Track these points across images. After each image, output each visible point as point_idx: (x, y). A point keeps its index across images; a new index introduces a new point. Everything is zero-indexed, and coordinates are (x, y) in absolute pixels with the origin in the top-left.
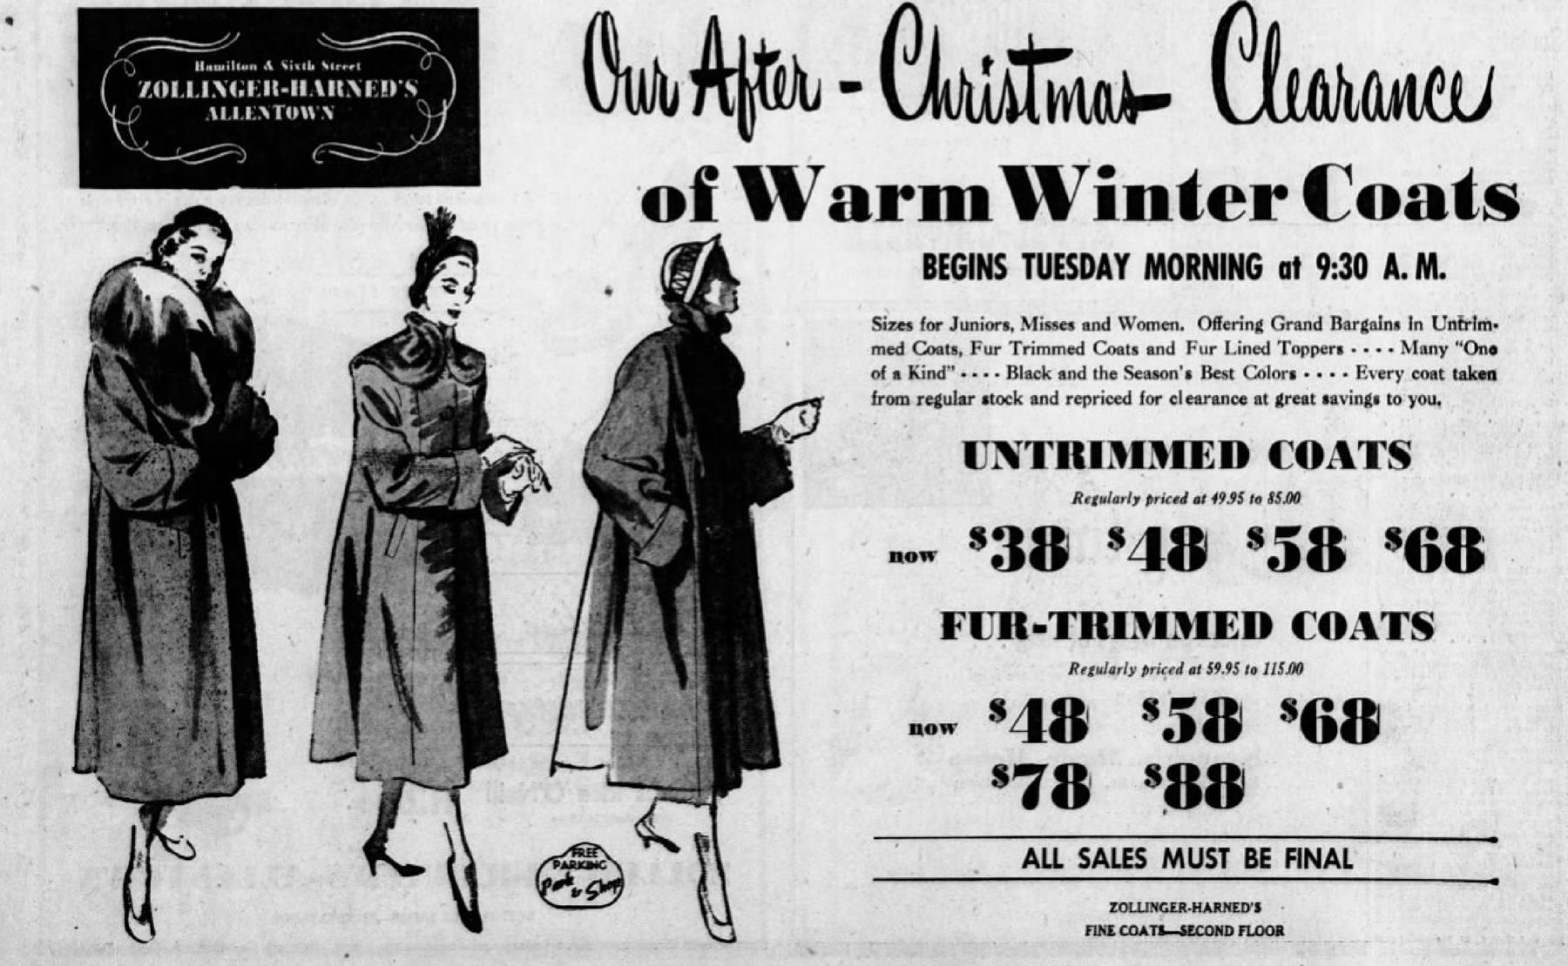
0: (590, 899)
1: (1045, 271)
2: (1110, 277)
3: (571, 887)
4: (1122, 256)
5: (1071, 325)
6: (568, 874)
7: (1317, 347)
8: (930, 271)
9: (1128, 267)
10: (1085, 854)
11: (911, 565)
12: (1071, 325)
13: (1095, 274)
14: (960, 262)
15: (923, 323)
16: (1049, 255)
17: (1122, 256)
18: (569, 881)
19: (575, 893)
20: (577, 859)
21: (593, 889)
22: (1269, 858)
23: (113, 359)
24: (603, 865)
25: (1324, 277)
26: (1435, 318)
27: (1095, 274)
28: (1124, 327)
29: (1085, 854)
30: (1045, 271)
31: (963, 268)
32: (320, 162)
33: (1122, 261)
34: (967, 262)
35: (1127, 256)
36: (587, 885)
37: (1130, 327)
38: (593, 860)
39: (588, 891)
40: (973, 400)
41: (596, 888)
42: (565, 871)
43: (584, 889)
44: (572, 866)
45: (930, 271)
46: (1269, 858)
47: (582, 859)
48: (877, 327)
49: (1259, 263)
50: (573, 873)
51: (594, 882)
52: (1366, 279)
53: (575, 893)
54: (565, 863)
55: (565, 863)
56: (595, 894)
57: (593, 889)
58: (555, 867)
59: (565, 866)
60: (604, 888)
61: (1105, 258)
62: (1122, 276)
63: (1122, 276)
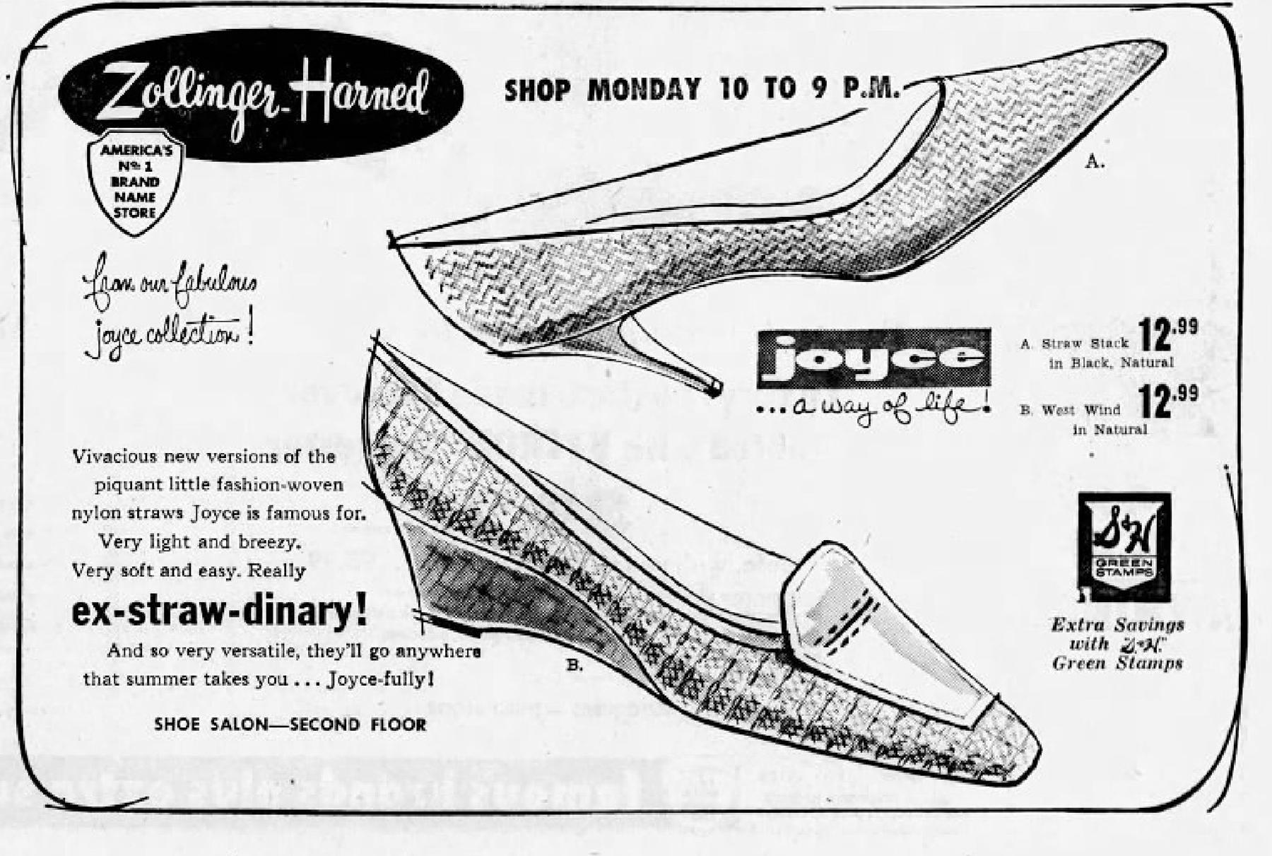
2: (680, 97)
5: (153, 456)
7: (406, 729)
9: (699, 91)
12: (153, 456)
15: (220, 482)
16: (270, 621)
22: (198, 724)
23: (479, 506)
26: (119, 517)
28: (1046, 412)
32: (427, 112)
33: (693, 84)
35: (697, 80)
37: (171, 517)
40: (195, 680)
46: (198, 724)
48: (1121, 666)
61: (675, 81)
62: (693, 96)
63: (693, 96)
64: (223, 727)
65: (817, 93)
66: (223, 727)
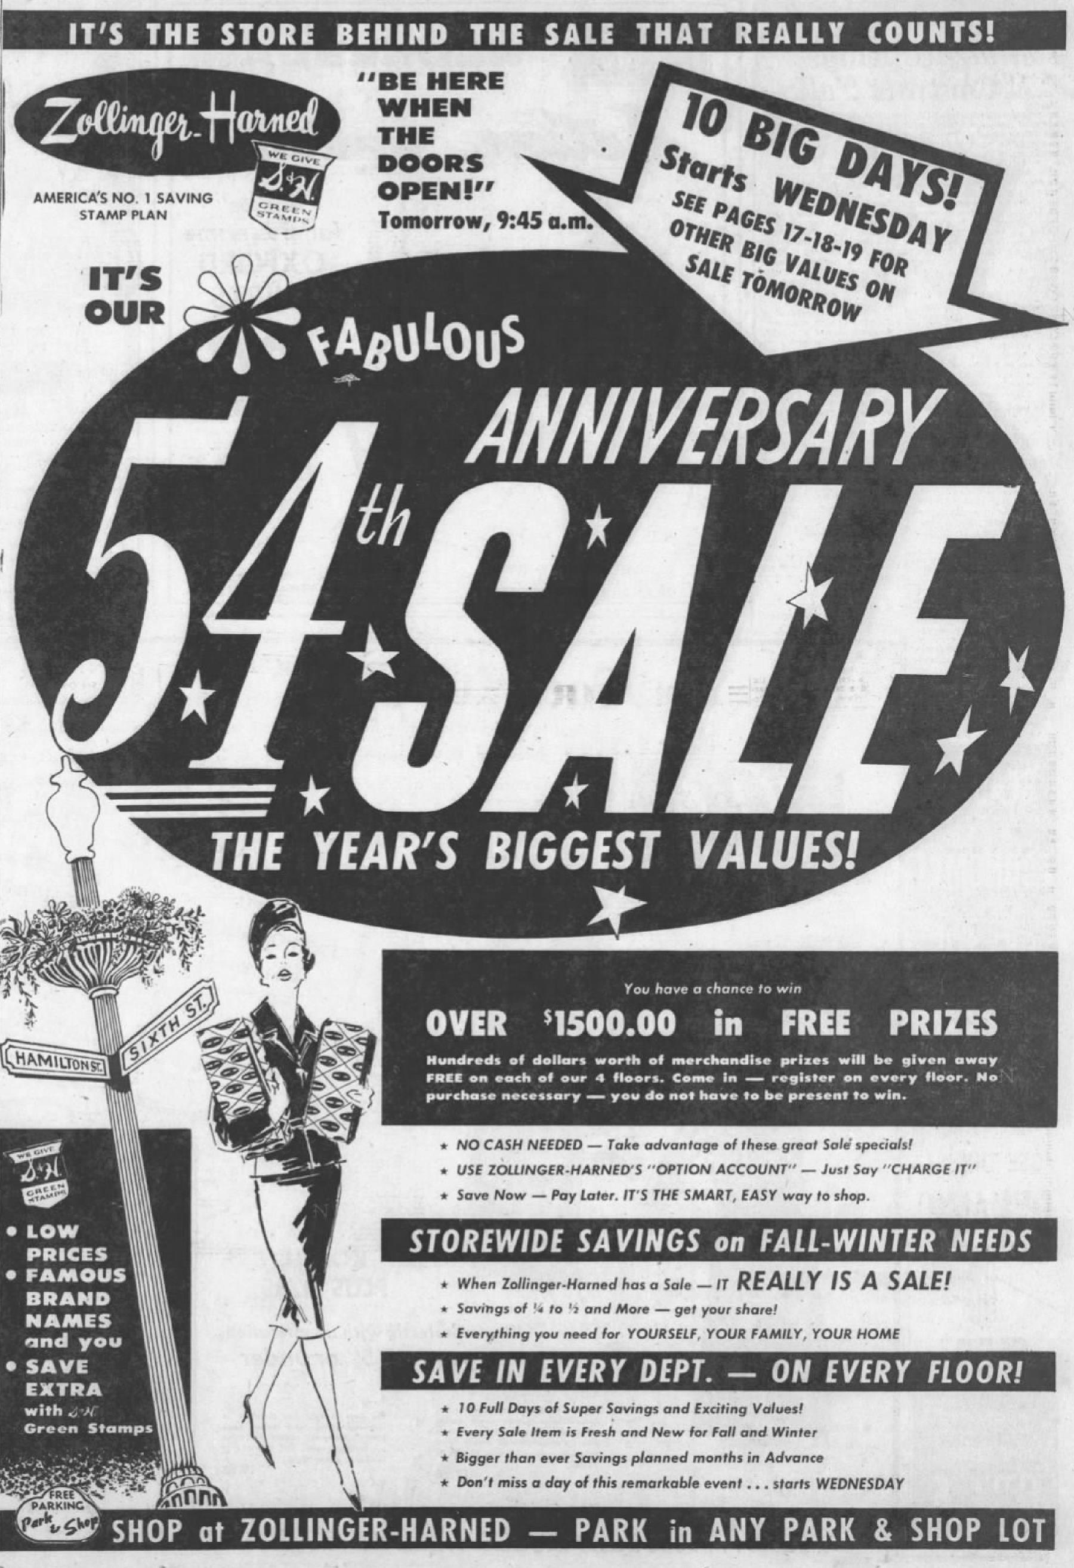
0: (69, 1534)
1: (829, 278)
3: (50, 1524)
4: (814, 1274)
6: (46, 1514)
8: (748, 253)
10: (895, 1276)
11: (468, 1202)
14: (749, 217)
17: (814, 1274)
18: (48, 1519)
19: (53, 1530)
20: (54, 1500)
21: (70, 1525)
24: (80, 1505)
25: (503, 227)
29: (895, 1276)
30: (829, 278)
31: (751, 221)
34: (754, 218)
36: (66, 1521)
38: (71, 1501)
39: (66, 1527)
41: (74, 1524)
42: (43, 1511)
43: (62, 1525)
44: (50, 1506)
45: (748, 253)
47: (59, 1500)
49: (813, 144)
50: (50, 1512)
51: (73, 1520)
52: (718, 138)
53: (53, 1530)
54: (43, 1504)
55: (43, 1504)
56: (74, 1530)
57: (70, 1525)
58: (34, 1508)
59: (43, 1506)
60: (81, 1525)
64: (906, 1285)
65: (500, 224)
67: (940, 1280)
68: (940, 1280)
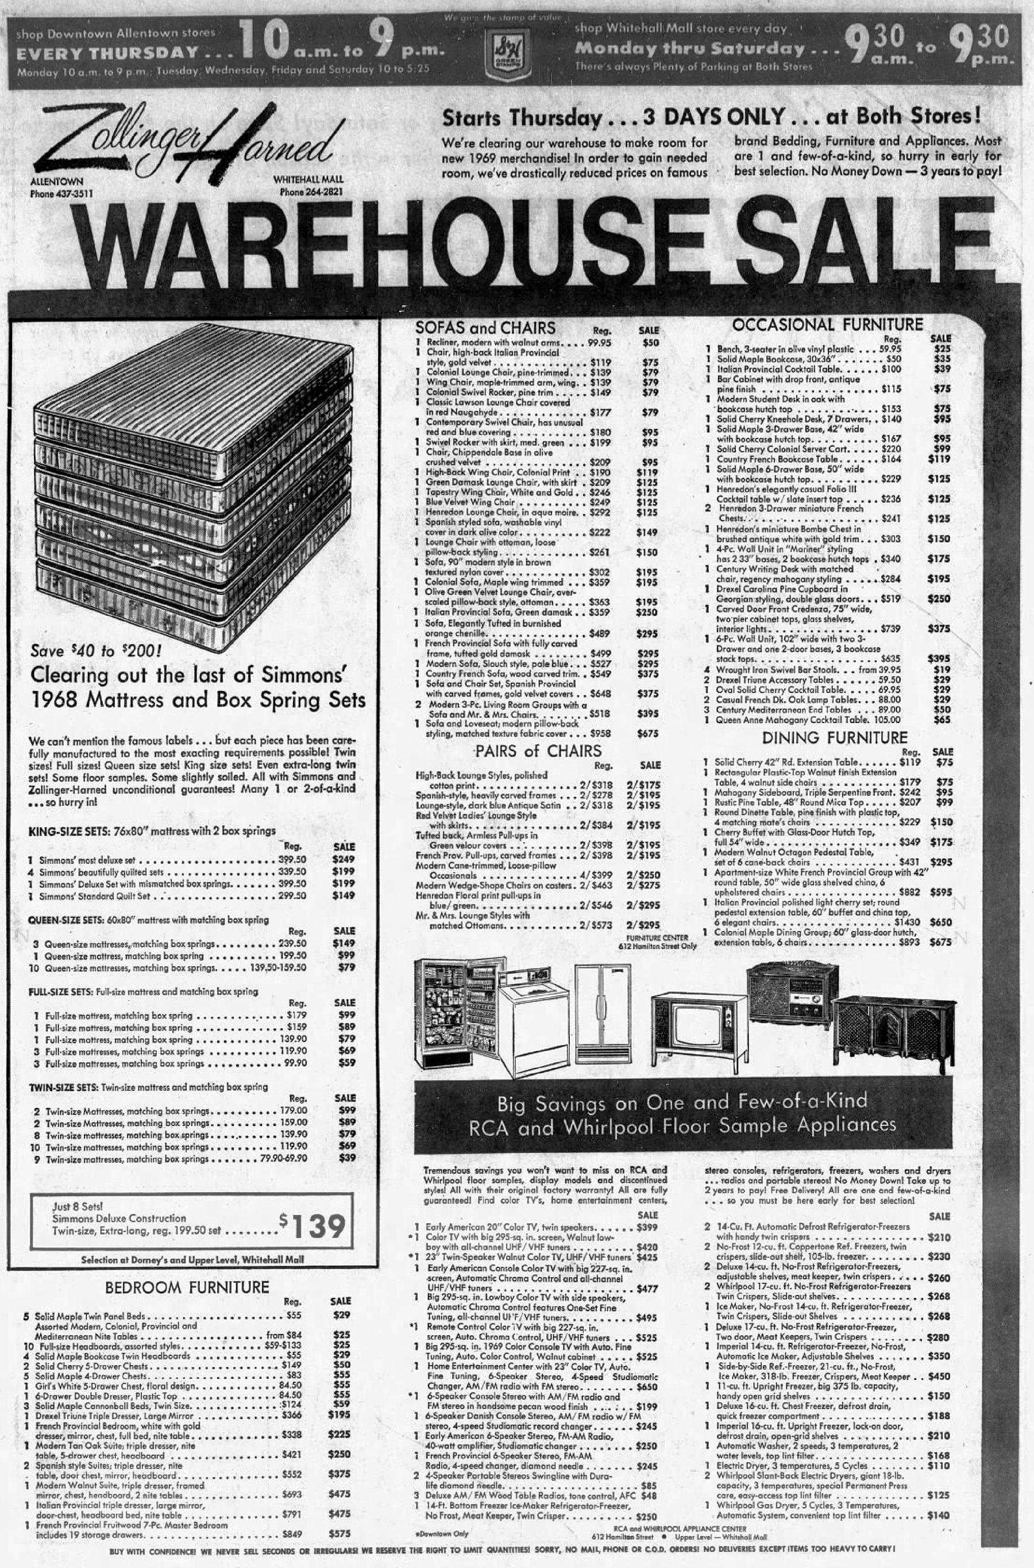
13: (429, 219)
27: (429, 219)
64: (684, 120)
66: (684, 120)
67: (339, 243)
68: (339, 243)
